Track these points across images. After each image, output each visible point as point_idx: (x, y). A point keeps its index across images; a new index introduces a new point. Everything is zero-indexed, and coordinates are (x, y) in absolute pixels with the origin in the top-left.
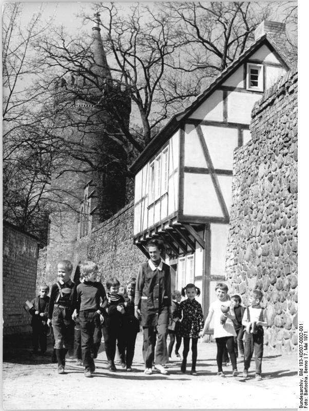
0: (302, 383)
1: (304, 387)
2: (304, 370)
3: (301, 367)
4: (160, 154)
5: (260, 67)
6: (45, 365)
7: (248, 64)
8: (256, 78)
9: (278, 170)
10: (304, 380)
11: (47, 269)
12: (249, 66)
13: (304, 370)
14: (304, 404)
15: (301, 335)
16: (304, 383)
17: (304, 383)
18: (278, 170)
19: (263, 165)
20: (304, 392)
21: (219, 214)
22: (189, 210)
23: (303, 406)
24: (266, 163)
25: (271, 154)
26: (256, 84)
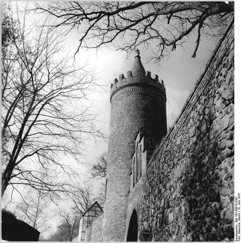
0: (237, 227)
1: (238, 229)
2: (238, 219)
3: (236, 217)
10: (238, 225)
13: (238, 219)
14: (238, 239)
16: (238, 226)
17: (238, 226)
20: (238, 232)
23: (238, 240)
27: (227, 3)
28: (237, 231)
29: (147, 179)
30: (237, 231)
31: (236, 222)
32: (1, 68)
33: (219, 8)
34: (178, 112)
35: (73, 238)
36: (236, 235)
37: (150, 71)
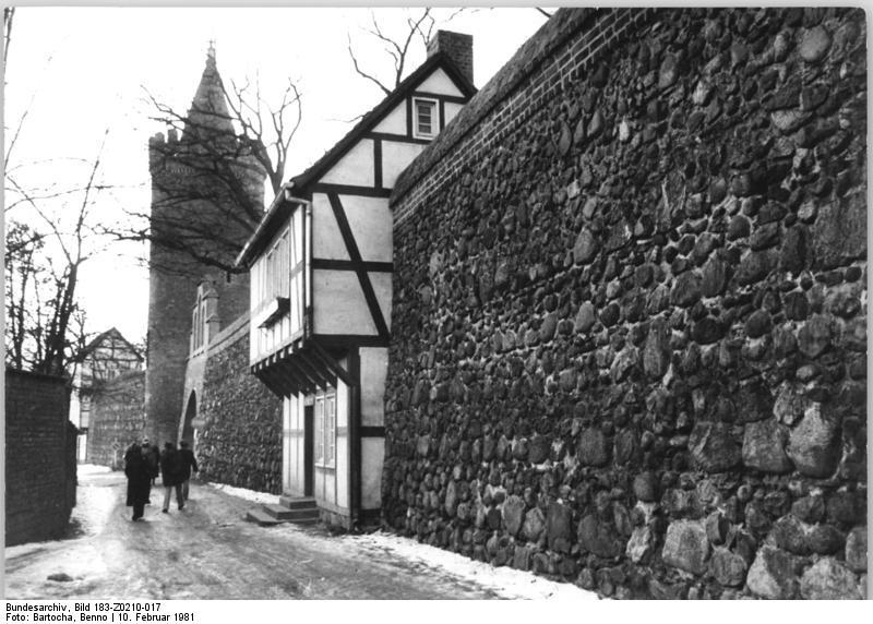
0: (58, 609)
1: (51, 613)
2: (87, 613)
3: (92, 607)
4: (280, 239)
5: (434, 103)
6: (98, 334)
7: (414, 99)
8: (428, 120)
9: (460, 264)
10: (66, 613)
11: (147, 401)
12: (416, 101)
13: (87, 613)
14: (15, 613)
15: (126, 607)
16: (60, 613)
17: (60, 613)
18: (460, 264)
19: (436, 255)
20: (40, 613)
21: (369, 329)
22: (326, 326)
23: (11, 612)
24: (440, 252)
25: (448, 237)
26: (428, 129)
27: (76, 513)
28: (43, 608)
29: (464, 218)
30: (43, 608)
31: (77, 607)
32: (3, 251)
33: (127, 472)
34: (389, 298)
35: (158, 275)
36: (30, 608)
37: (110, 328)
